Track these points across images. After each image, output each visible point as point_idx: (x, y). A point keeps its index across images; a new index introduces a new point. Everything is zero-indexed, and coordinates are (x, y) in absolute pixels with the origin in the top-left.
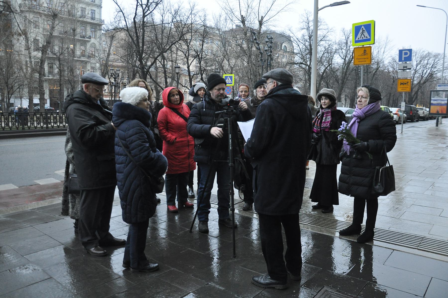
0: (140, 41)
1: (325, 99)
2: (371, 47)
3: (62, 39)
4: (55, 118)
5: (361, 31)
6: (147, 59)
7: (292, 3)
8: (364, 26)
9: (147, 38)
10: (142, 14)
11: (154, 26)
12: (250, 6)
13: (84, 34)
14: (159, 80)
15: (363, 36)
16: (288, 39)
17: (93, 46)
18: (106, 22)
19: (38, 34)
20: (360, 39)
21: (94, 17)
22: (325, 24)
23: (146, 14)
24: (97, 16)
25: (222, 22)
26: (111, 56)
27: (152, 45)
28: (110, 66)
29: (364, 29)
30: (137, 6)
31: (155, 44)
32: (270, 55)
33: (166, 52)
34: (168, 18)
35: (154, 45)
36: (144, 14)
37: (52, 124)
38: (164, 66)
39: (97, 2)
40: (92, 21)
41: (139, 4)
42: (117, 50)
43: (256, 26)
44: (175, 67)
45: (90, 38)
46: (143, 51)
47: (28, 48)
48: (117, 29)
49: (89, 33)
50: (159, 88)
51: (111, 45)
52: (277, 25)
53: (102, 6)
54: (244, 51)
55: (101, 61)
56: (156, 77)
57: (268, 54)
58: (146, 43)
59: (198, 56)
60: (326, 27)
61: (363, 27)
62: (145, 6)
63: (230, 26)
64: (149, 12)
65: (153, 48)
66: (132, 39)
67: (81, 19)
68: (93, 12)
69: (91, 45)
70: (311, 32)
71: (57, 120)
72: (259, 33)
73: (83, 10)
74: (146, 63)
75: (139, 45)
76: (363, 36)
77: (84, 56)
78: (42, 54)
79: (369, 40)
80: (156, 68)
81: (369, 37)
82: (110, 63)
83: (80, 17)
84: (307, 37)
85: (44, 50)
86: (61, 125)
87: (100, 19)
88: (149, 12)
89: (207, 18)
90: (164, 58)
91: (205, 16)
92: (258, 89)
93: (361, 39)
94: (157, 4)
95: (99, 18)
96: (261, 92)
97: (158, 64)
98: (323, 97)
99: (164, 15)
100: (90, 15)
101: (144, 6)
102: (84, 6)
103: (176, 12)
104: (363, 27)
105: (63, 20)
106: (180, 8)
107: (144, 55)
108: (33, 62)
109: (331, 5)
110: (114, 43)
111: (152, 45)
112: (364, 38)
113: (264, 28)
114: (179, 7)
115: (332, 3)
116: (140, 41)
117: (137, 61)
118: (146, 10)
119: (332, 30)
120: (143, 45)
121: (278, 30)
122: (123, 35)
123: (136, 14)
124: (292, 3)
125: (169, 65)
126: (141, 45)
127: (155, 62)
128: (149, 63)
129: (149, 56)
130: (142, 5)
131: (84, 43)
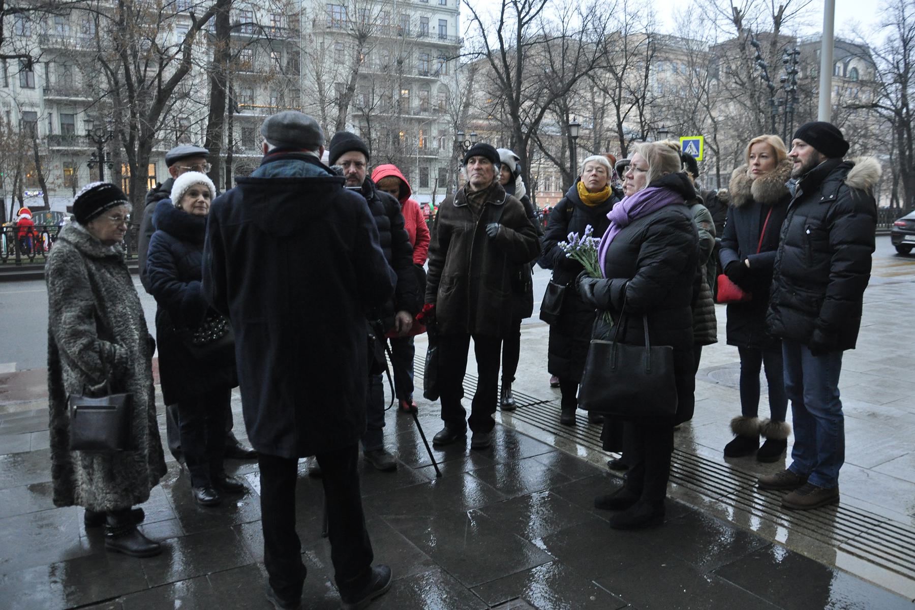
21: (444, 33)
23: (524, 20)
24: (450, 32)
25: (694, 25)
34: (575, 24)
36: (520, 20)
39: (450, 5)
40: (441, 42)
45: (437, 74)
57: (788, 89)
59: (639, 101)
68: (443, 24)
73: (425, 22)
77: (425, 110)
78: (340, 110)
83: (419, 36)
84: (898, 44)
89: (657, 17)
91: (651, 15)
92: (469, 165)
95: (454, 34)
96: (474, 172)
99: (566, 20)
100: (437, 31)
105: (385, 43)
113: (785, 30)
120: (519, 83)
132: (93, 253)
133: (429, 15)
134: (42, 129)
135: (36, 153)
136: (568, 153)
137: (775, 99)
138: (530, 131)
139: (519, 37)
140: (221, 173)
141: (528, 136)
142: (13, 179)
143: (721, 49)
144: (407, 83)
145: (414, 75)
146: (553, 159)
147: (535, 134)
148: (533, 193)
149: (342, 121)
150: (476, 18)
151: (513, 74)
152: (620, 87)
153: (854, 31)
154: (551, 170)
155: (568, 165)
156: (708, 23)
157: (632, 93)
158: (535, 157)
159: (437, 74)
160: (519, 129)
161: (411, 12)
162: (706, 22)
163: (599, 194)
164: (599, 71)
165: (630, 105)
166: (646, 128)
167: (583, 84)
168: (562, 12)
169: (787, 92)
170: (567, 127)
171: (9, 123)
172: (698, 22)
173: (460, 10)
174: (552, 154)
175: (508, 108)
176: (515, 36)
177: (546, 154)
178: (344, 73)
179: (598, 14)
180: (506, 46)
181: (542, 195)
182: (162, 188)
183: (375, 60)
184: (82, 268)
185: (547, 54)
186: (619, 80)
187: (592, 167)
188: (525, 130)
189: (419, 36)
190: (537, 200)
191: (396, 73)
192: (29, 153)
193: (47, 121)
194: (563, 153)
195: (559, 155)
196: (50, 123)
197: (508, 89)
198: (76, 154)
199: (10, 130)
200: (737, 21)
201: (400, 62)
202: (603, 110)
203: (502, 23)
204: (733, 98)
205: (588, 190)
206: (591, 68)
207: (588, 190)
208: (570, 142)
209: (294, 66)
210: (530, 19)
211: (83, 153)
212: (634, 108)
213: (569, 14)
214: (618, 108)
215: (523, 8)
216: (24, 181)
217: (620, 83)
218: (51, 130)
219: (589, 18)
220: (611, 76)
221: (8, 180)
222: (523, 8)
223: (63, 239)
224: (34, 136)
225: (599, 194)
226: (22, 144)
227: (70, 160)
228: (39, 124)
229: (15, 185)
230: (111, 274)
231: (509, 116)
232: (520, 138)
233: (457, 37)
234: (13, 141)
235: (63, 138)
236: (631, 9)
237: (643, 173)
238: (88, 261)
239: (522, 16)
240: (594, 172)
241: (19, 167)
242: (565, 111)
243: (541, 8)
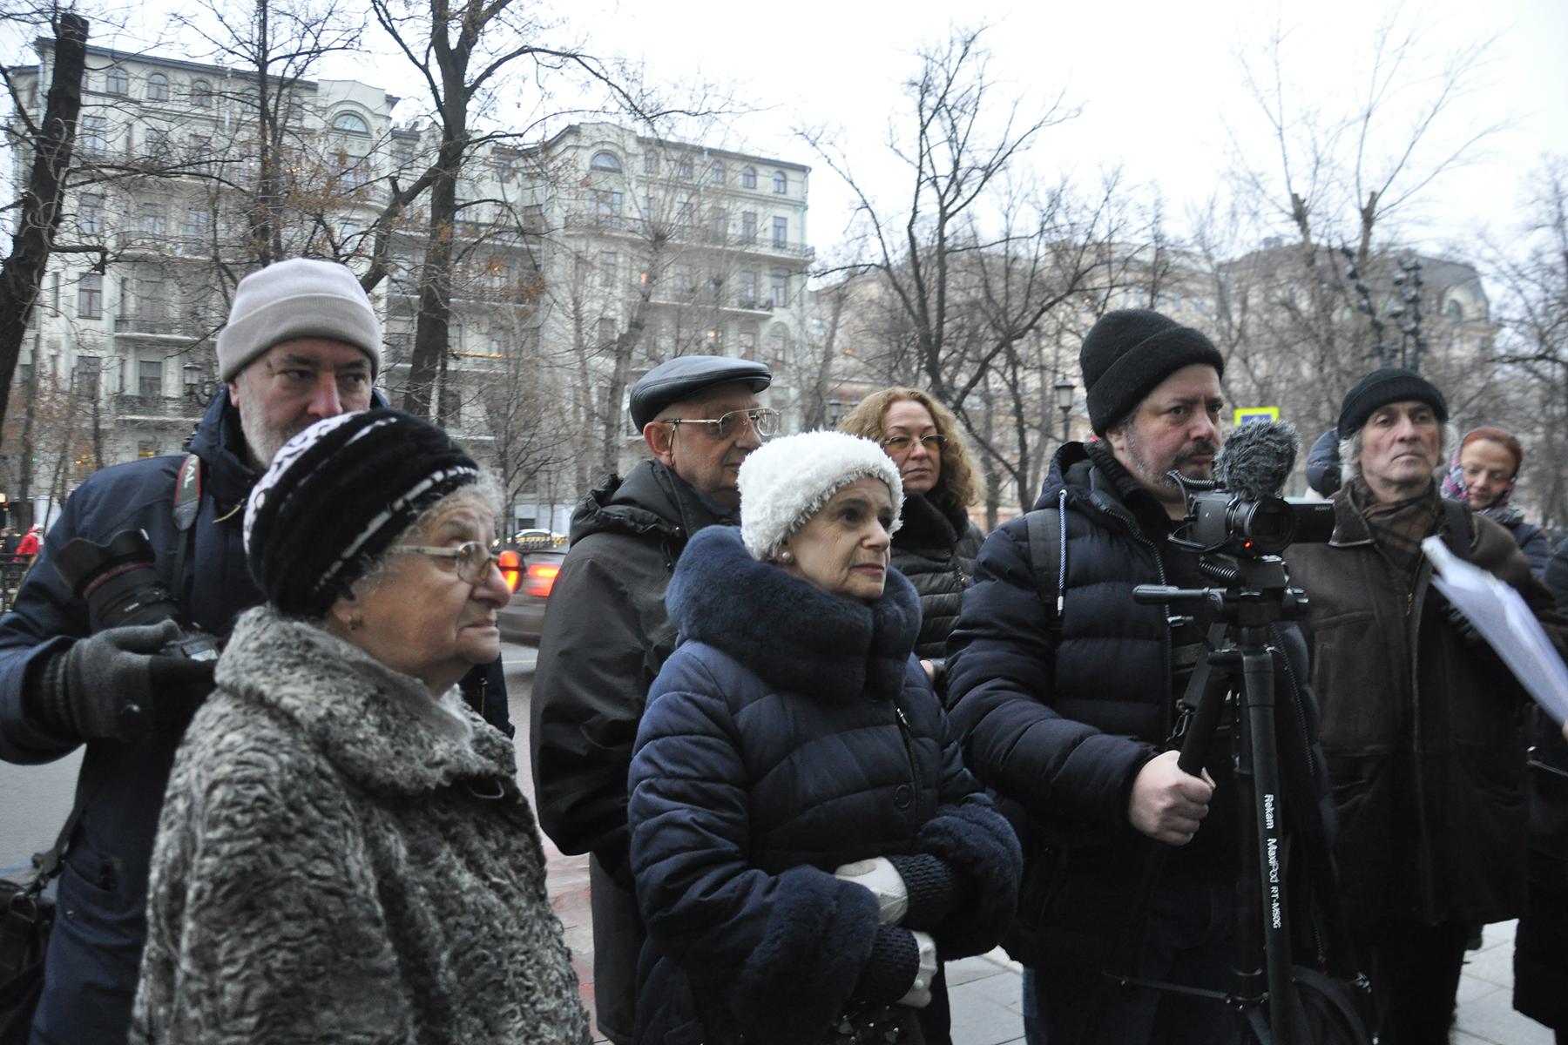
0: (933, 299)
3: (679, 311)
6: (958, 366)
7: (1494, 129)
9: (955, 296)
10: (938, 208)
11: (978, 260)
13: (750, 294)
14: (996, 439)
16: (1468, 276)
17: (781, 332)
18: (819, 253)
19: (610, 302)
23: (950, 210)
24: (792, 237)
26: (834, 362)
27: (972, 318)
28: (831, 394)
30: (919, 183)
31: (984, 311)
32: (1415, 332)
33: (1020, 336)
34: (1027, 221)
35: (979, 316)
36: (943, 210)
38: (1014, 386)
40: (777, 254)
42: (853, 340)
43: (1349, 231)
44: (1058, 388)
45: (769, 305)
46: (940, 335)
47: (579, 347)
48: (854, 272)
49: (767, 290)
50: (999, 467)
51: (834, 325)
52: (1418, 229)
53: (809, 202)
55: (804, 377)
56: (989, 427)
57: (1407, 328)
58: (950, 310)
62: (947, 181)
63: (1240, 241)
64: (960, 202)
65: (977, 328)
66: (905, 299)
68: (780, 225)
69: (774, 328)
72: (1364, 251)
73: (749, 220)
74: (952, 379)
75: (927, 321)
78: (618, 361)
80: (988, 399)
82: (831, 386)
85: (621, 350)
87: (803, 245)
88: (960, 202)
89: (1165, 211)
90: (1014, 362)
94: (988, 173)
97: (995, 382)
100: (770, 235)
101: (943, 183)
102: (748, 207)
103: (1054, 200)
105: (684, 254)
106: (1068, 186)
107: (942, 355)
108: (594, 389)
110: (846, 316)
111: (972, 318)
113: (1379, 234)
114: (1065, 181)
116: (933, 299)
117: (923, 373)
120: (941, 324)
121: (1429, 248)
122: (874, 290)
123: (915, 212)
124: (1494, 129)
125: (1032, 381)
126: (933, 316)
127: (982, 373)
128: (962, 380)
129: (963, 354)
131: (751, 324)
132: (399, 772)
133: (760, 210)
134: (107, 383)
135: (96, 424)
137: (1383, 344)
140: (1257, 421)
142: (53, 468)
145: (732, 307)
153: (1481, 236)
156: (1244, 220)
159: (769, 305)
171: (54, 374)
182: (620, 493)
184: (358, 861)
189: (740, 243)
192: (84, 425)
193: (117, 372)
196: (122, 377)
198: (162, 428)
199: (55, 383)
203: (915, 212)
211: (174, 425)
213: (1017, 203)
216: (71, 471)
218: (122, 389)
221: (44, 470)
223: (254, 701)
224: (93, 397)
226: (72, 409)
227: (150, 438)
228: (104, 378)
229: (55, 479)
230: (474, 865)
234: (59, 403)
235: (142, 400)
238: (379, 816)
241: (64, 448)
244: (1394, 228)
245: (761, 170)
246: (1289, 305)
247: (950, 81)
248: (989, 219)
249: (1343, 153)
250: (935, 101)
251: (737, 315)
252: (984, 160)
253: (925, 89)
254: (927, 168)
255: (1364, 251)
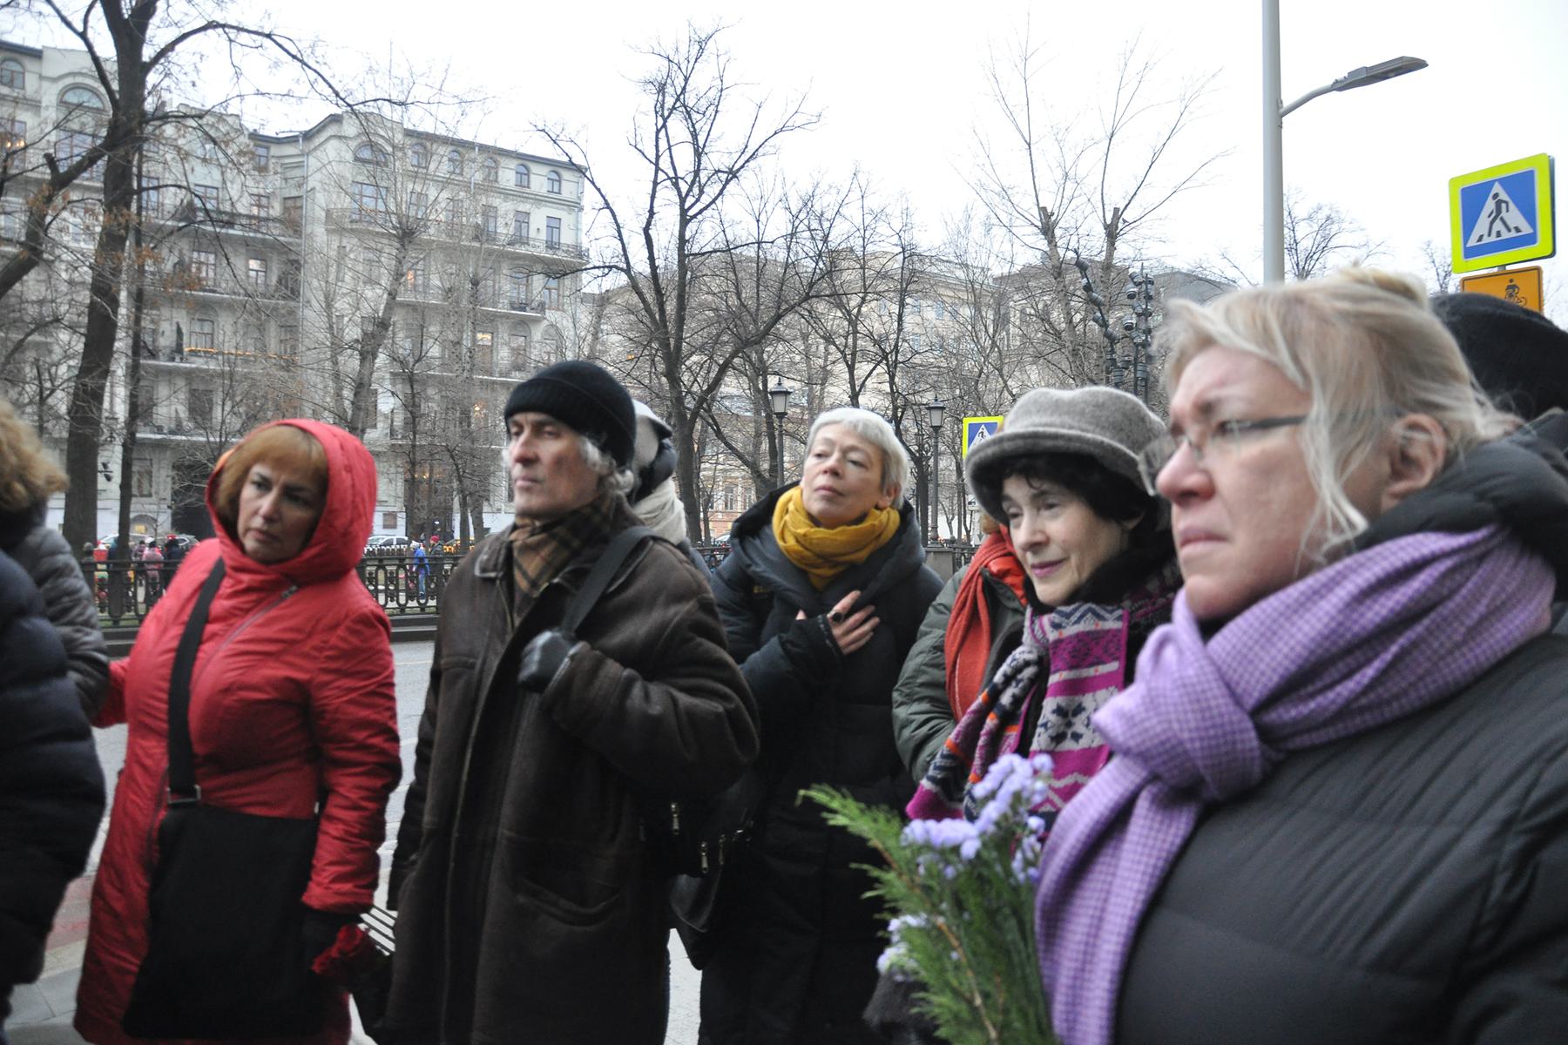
1: (1041, 503)
2: (1538, 269)
4: (392, 579)
5: (1490, 205)
8: (1504, 182)
10: (677, 210)
12: (1071, 174)
15: (1498, 226)
20: (1486, 240)
22: (1352, 227)
23: (691, 213)
24: (567, 238)
25: (977, 232)
29: (1503, 196)
30: (655, 183)
34: (777, 226)
36: (684, 212)
37: (402, 600)
40: (548, 255)
41: (661, 176)
43: (1094, 246)
45: (542, 307)
52: (1143, 250)
54: (1058, 334)
57: (1138, 340)
59: (888, 356)
60: (1358, 238)
61: (1497, 188)
67: (510, 249)
68: (554, 225)
70: (1302, 257)
71: (397, 586)
73: (522, 219)
76: (1498, 226)
78: (363, 360)
79: (1531, 239)
81: (1526, 229)
83: (511, 244)
86: (410, 604)
89: (916, 220)
91: (906, 212)
93: (1493, 238)
98: (1016, 490)
99: (763, 218)
100: (543, 236)
102: (523, 207)
104: (1497, 188)
105: (451, 251)
109: (1342, 86)
112: (1505, 235)
113: (1123, 250)
115: (1341, 74)
118: (690, 200)
119: (1381, 249)
120: (681, 320)
123: (652, 213)
130: (675, 181)
136: (765, 446)
138: (699, 406)
139: (682, 241)
141: (695, 414)
143: (1022, 280)
144: (491, 322)
145: (503, 308)
146: (740, 457)
147: (709, 410)
148: (705, 513)
149: (366, 379)
150: (608, 206)
151: (671, 307)
152: (856, 332)
154: (736, 474)
155: (765, 466)
157: (876, 342)
158: (709, 451)
160: (679, 400)
161: (497, 201)
162: (995, 230)
163: (841, 534)
164: (821, 307)
165: (871, 366)
166: (900, 402)
167: (791, 324)
168: (756, 204)
169: (1137, 345)
170: (763, 399)
172: (982, 230)
173: (584, 203)
174: (739, 446)
175: (661, 367)
176: (675, 241)
177: (727, 444)
178: (375, 298)
179: (817, 209)
180: (659, 262)
181: (720, 516)
183: (431, 281)
185: (731, 275)
186: (853, 322)
187: (830, 443)
188: (690, 403)
189: (511, 244)
190: (711, 525)
191: (469, 305)
194: (757, 446)
195: (750, 448)
197: (662, 330)
200: (1048, 230)
201: (475, 283)
202: (826, 376)
203: (652, 213)
204: (1038, 356)
205: (814, 520)
206: (807, 298)
207: (814, 520)
208: (770, 424)
209: (290, 287)
210: (700, 212)
212: (879, 370)
213: (769, 207)
214: (851, 369)
215: (690, 190)
217: (855, 327)
219: (802, 216)
220: (839, 314)
222: (690, 190)
225: (841, 534)
231: (664, 380)
232: (682, 416)
233: (577, 247)
236: (872, 202)
237: (1276, 440)
239: (687, 205)
240: (831, 462)
242: (761, 371)
243: (721, 193)
244: (1139, 245)
245: (534, 168)
246: (1044, 317)
247: (686, 79)
248: (733, 220)
249: (1089, 167)
250: (672, 100)
251: (507, 316)
252: (725, 162)
253: (662, 89)
254: (665, 163)
255: (1108, 266)
